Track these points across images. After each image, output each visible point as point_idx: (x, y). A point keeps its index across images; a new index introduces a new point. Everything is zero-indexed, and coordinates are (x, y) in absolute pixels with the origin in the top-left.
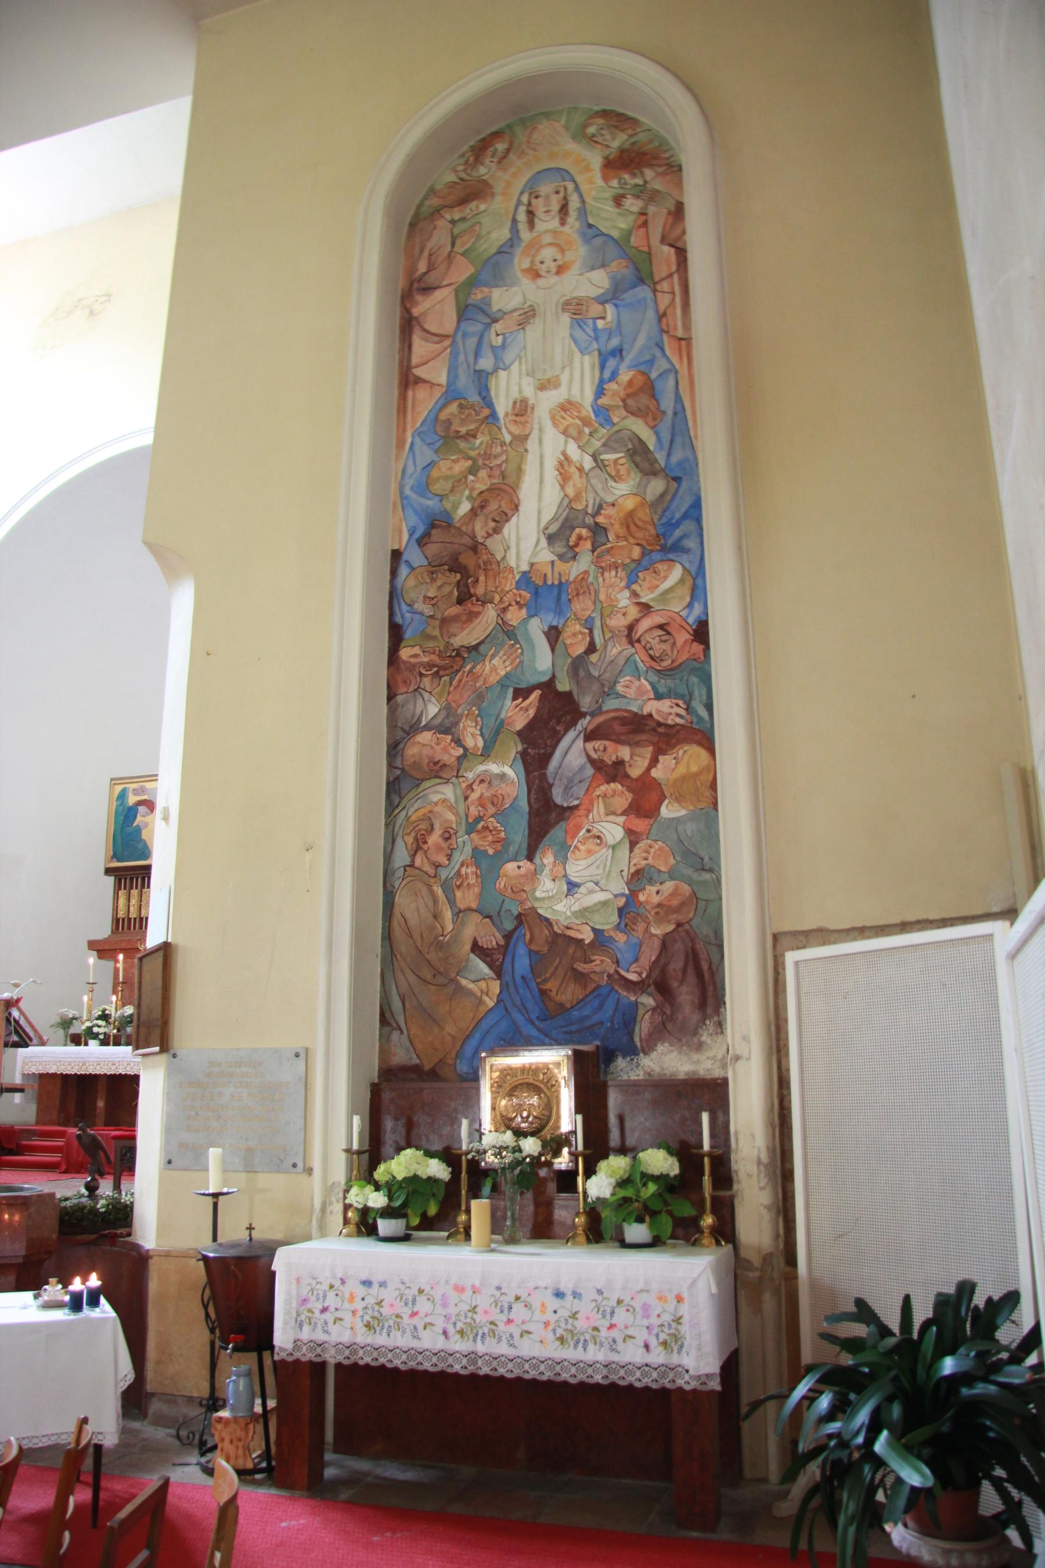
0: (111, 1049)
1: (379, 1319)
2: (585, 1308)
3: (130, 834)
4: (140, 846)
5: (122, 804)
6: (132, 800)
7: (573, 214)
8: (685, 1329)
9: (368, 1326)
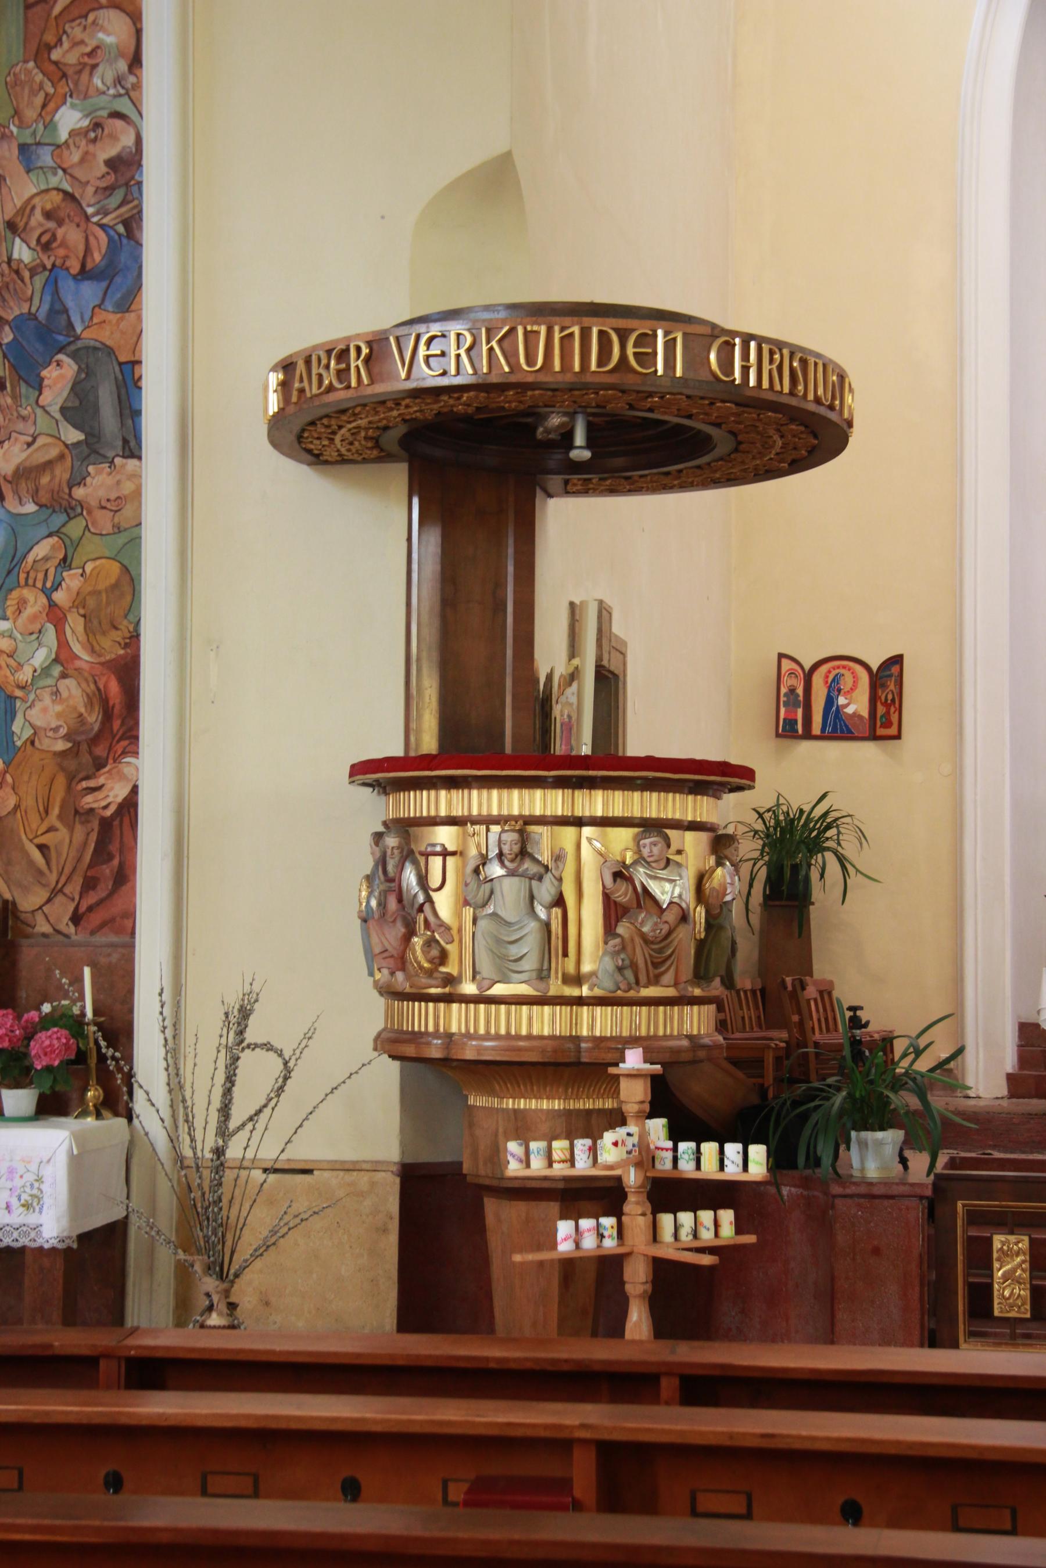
7: (92, 783)
8: (43, 1187)
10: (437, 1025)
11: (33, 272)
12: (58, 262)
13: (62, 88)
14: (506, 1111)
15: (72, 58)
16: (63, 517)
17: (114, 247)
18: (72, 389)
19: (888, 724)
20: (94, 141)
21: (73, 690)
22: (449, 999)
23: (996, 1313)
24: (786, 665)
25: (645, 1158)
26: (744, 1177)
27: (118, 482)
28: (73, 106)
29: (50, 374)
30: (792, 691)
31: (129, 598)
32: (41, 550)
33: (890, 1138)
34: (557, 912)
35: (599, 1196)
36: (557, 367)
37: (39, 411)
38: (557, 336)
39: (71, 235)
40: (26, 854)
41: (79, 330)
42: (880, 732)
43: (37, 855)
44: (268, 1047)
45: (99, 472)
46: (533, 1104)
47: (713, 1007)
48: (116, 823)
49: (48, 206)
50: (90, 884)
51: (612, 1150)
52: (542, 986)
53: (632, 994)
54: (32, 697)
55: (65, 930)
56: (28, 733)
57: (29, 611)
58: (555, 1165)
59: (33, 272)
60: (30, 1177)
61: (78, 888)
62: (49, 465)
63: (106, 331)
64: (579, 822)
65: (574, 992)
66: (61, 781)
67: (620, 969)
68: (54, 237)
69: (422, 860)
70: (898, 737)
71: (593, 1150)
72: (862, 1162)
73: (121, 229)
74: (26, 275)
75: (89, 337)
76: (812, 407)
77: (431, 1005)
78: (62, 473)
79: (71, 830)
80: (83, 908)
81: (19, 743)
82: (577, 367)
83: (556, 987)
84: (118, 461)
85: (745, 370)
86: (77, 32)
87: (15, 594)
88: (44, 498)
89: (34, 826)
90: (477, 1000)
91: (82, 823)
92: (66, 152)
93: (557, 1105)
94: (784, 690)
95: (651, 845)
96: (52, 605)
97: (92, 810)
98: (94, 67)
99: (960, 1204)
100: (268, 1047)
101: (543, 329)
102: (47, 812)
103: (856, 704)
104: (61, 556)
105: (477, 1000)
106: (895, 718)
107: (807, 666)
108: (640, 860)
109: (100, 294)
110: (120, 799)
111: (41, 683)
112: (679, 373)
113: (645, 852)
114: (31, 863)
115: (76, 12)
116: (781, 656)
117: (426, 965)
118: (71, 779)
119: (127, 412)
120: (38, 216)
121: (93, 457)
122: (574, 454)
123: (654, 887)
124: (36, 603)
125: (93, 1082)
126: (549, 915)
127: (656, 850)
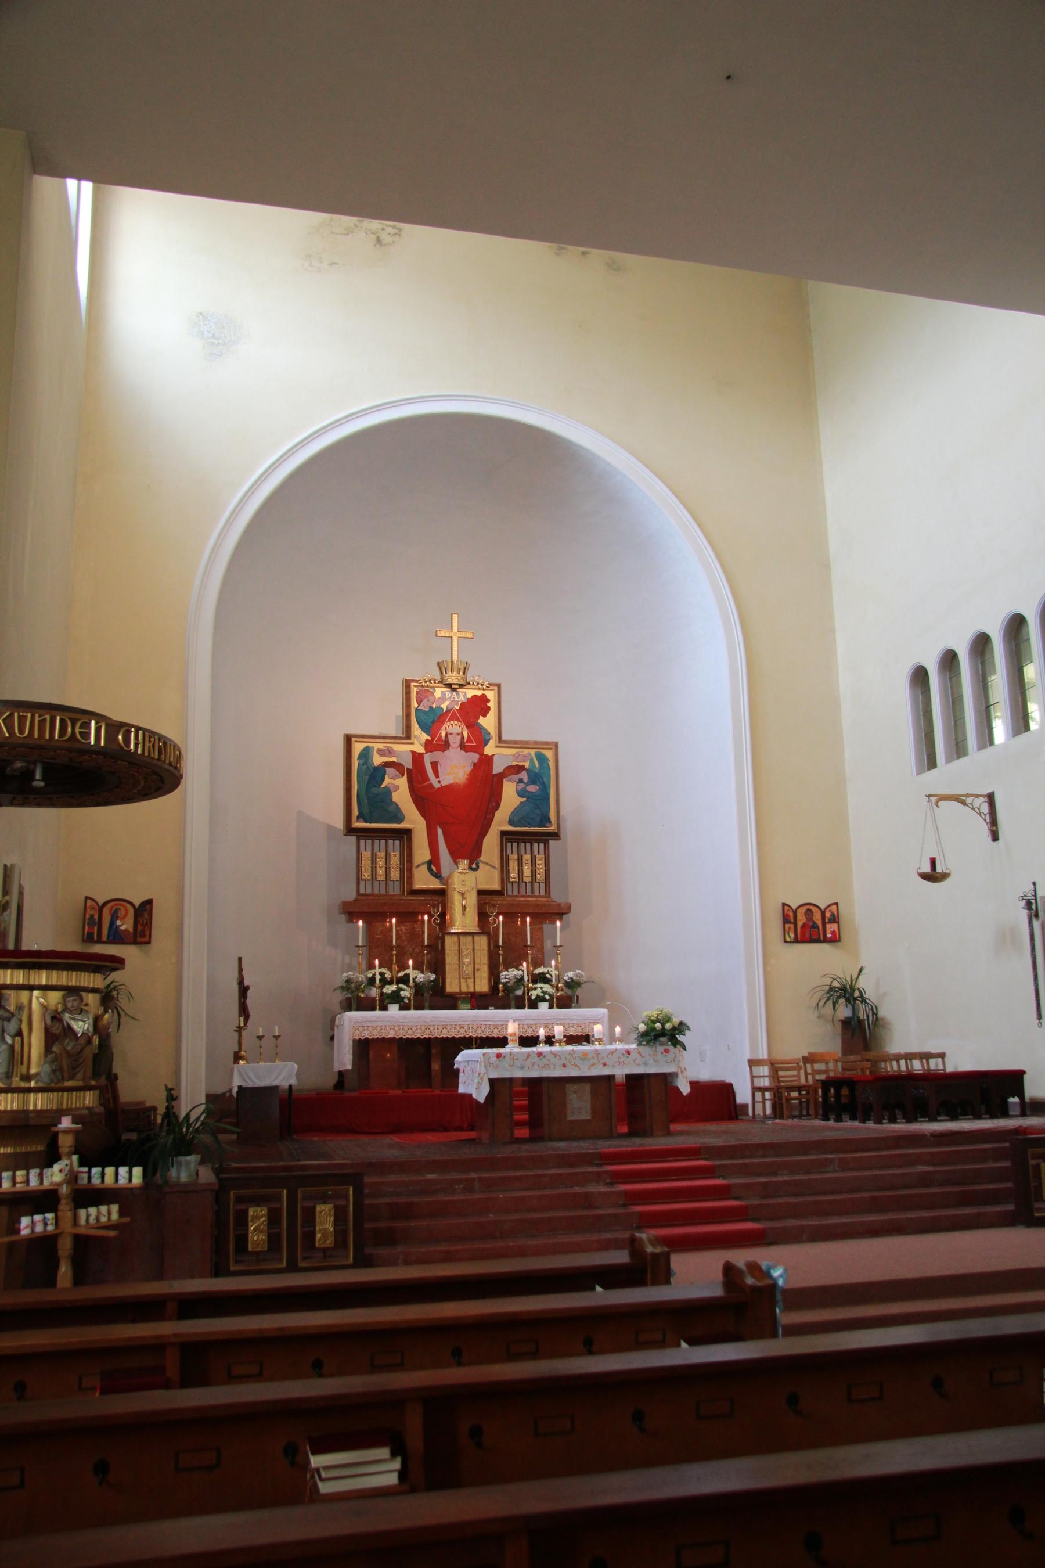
0: (412, 1013)
3: (377, 795)
4: (391, 808)
5: (365, 763)
6: (378, 760)
19: (144, 936)
23: (250, 1249)
24: (89, 903)
25: (72, 1178)
26: (130, 1186)
30: (92, 916)
33: (193, 1159)
34: (18, 1039)
35: (44, 1201)
36: (36, 735)
38: (37, 719)
42: (139, 940)
47: (97, 1092)
51: (55, 1175)
53: (60, 1085)
58: (18, 1185)
64: (31, 988)
65: (23, 1084)
67: (54, 1071)
70: (149, 942)
71: (41, 1176)
72: (179, 1173)
76: (167, 767)
82: (47, 737)
83: (16, 1082)
85: (136, 745)
93: (9, 1150)
94: (87, 916)
95: (71, 1001)
99: (232, 1193)
101: (29, 715)
103: (126, 925)
106: (147, 934)
107: (101, 903)
108: (66, 1009)
112: (102, 744)
113: (69, 1005)
116: (87, 898)
122: (34, 784)
123: (73, 1024)
126: (13, 1041)
127: (75, 1004)
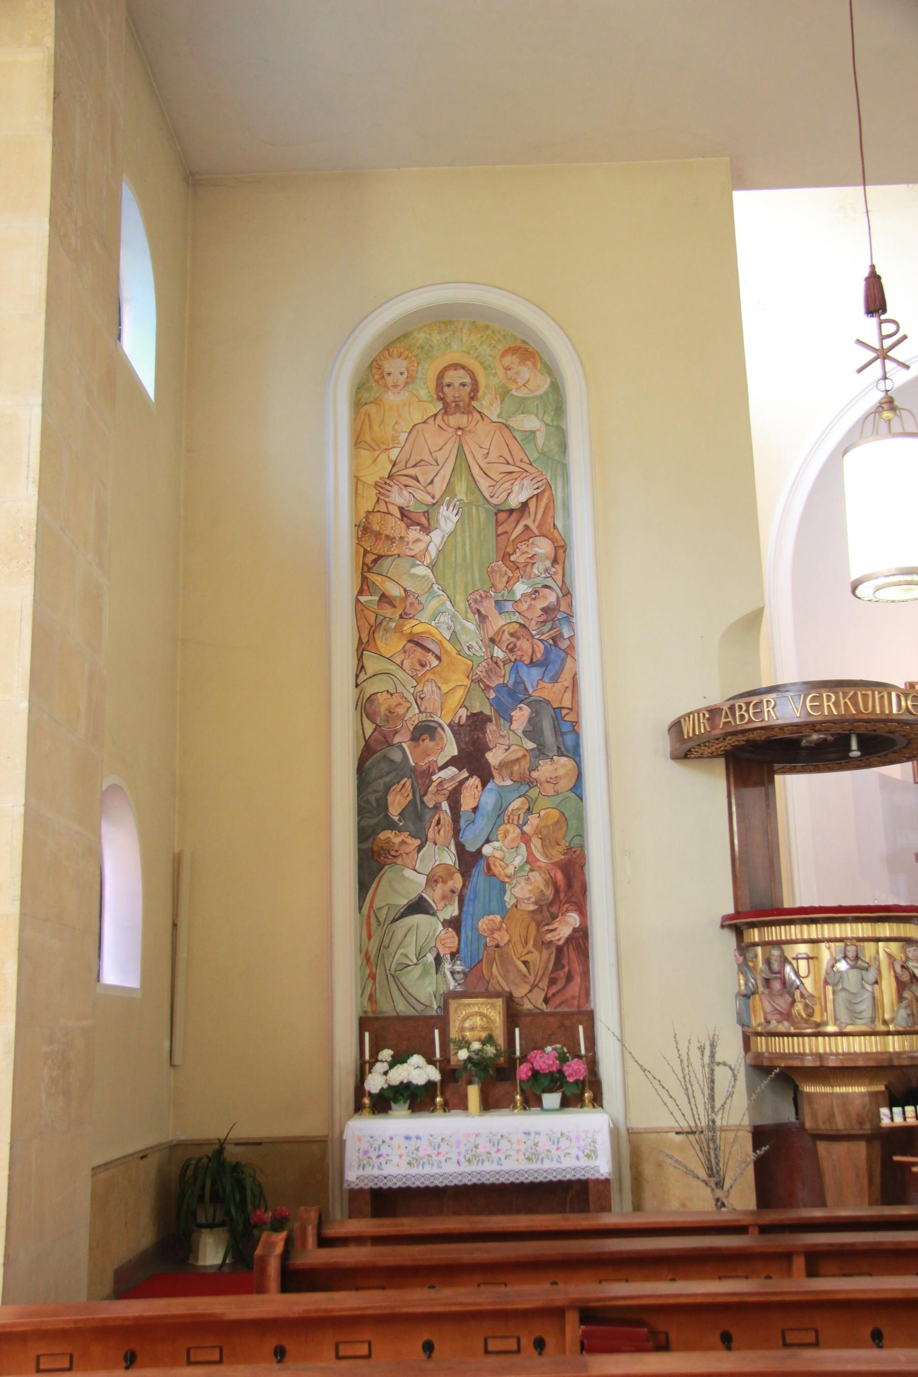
1: (536, 1154)
2: (423, 1144)
7: (550, 927)
8: (597, 1146)
9: (409, 1163)
10: (811, 1049)
11: (505, 663)
12: (518, 658)
13: (517, 574)
14: (837, 1094)
15: (522, 560)
16: (527, 787)
17: (547, 651)
18: (529, 721)
20: (535, 599)
21: (537, 878)
22: (816, 1035)
27: (556, 769)
28: (523, 582)
29: (516, 714)
31: (565, 829)
32: (516, 804)
36: (878, 711)
37: (511, 733)
38: (877, 696)
39: (524, 645)
40: (516, 967)
41: (531, 692)
43: (522, 967)
44: (725, 1064)
45: (546, 764)
46: (850, 1089)
48: (565, 948)
49: (512, 631)
50: (553, 981)
52: (872, 1026)
54: (515, 881)
55: (540, 1007)
56: (513, 901)
57: (511, 836)
59: (505, 663)
60: (589, 1140)
61: (546, 984)
62: (517, 760)
63: (549, 692)
64: (877, 940)
66: (533, 927)
67: (908, 1015)
68: (515, 646)
69: (794, 962)
73: (551, 642)
74: (501, 664)
75: (536, 695)
77: (795, 1038)
78: (525, 764)
79: (541, 952)
80: (550, 995)
81: (508, 907)
84: (555, 758)
86: (523, 547)
87: (502, 827)
88: (516, 777)
89: (520, 951)
90: (835, 1035)
91: (547, 949)
92: (520, 605)
93: (863, 1089)
96: (523, 833)
97: (551, 942)
98: (534, 564)
100: (725, 1064)
102: (526, 943)
104: (527, 807)
105: (835, 1035)
109: (541, 673)
110: (566, 935)
111: (519, 875)
113: (910, 955)
114: (519, 971)
115: (523, 538)
117: (804, 1016)
118: (539, 925)
119: (559, 733)
120: (506, 635)
121: (541, 757)
124: (514, 832)
125: (587, 1088)
126: (873, 989)
